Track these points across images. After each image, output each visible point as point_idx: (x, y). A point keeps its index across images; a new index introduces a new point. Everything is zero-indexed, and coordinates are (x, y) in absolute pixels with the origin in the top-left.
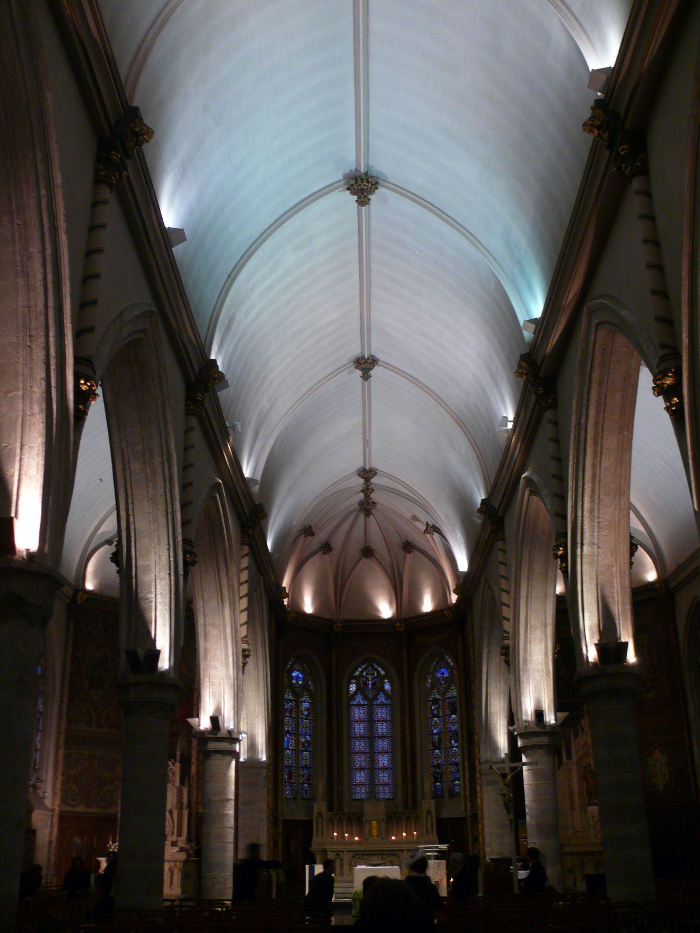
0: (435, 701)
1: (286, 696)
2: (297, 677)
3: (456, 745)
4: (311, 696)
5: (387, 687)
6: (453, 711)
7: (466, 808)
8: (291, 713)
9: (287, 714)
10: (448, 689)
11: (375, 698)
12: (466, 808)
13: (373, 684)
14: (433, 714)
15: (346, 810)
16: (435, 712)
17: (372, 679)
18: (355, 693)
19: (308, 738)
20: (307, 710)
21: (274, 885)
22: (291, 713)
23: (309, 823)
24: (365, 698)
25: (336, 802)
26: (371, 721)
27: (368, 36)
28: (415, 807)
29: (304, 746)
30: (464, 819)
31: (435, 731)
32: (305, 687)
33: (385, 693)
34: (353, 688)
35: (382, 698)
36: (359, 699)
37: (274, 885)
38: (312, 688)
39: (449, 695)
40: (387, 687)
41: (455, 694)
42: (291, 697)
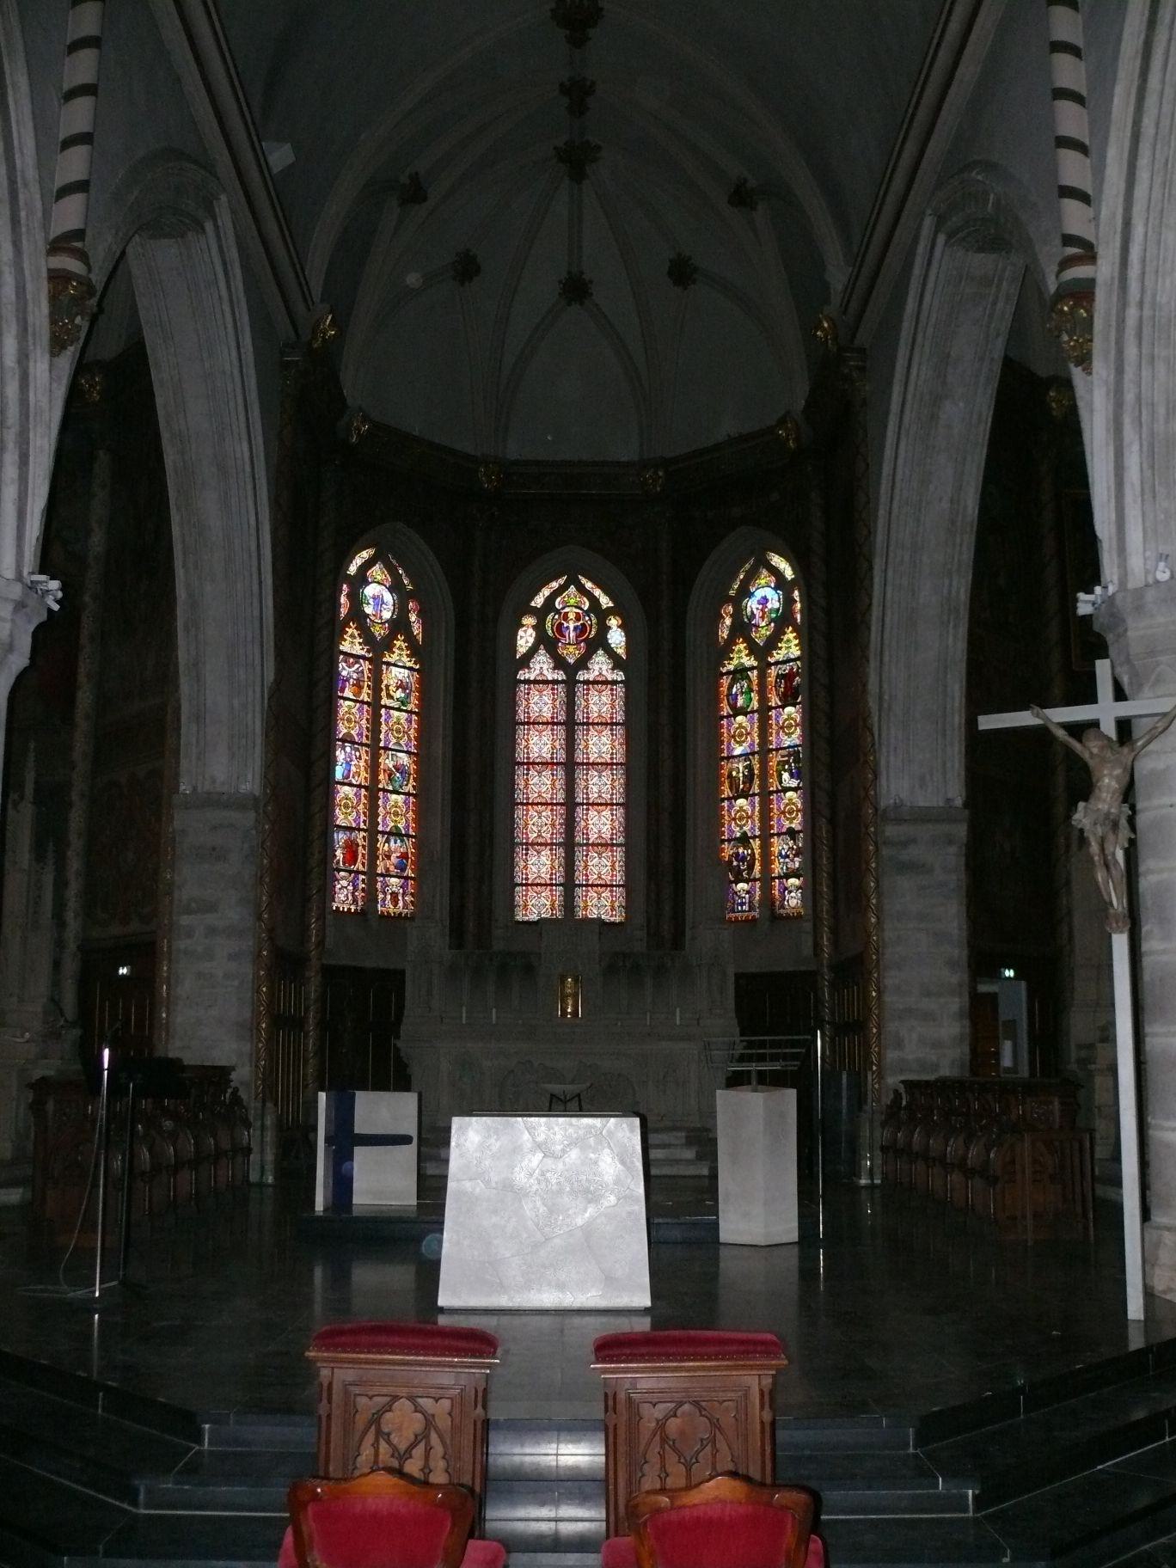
0: (741, 672)
1: (345, 647)
2: (378, 600)
3: (794, 783)
4: (415, 650)
5: (617, 638)
6: (788, 699)
7: (817, 946)
8: (358, 685)
9: (348, 693)
10: (773, 642)
11: (583, 663)
12: (817, 946)
13: (581, 630)
14: (733, 706)
15: (498, 946)
16: (740, 702)
17: (578, 618)
18: (533, 651)
19: (404, 759)
20: (401, 686)
21: (76, 843)
22: (358, 685)
23: (394, 979)
24: (559, 663)
25: (471, 925)
26: (571, 725)
27: (679, 739)
28: (678, 941)
29: (391, 778)
30: (811, 977)
31: (738, 751)
32: (399, 625)
33: (610, 653)
34: (525, 638)
35: (600, 665)
36: (542, 666)
37: (76, 843)
38: (417, 629)
39: (778, 656)
40: (617, 638)
41: (795, 652)
42: (358, 650)
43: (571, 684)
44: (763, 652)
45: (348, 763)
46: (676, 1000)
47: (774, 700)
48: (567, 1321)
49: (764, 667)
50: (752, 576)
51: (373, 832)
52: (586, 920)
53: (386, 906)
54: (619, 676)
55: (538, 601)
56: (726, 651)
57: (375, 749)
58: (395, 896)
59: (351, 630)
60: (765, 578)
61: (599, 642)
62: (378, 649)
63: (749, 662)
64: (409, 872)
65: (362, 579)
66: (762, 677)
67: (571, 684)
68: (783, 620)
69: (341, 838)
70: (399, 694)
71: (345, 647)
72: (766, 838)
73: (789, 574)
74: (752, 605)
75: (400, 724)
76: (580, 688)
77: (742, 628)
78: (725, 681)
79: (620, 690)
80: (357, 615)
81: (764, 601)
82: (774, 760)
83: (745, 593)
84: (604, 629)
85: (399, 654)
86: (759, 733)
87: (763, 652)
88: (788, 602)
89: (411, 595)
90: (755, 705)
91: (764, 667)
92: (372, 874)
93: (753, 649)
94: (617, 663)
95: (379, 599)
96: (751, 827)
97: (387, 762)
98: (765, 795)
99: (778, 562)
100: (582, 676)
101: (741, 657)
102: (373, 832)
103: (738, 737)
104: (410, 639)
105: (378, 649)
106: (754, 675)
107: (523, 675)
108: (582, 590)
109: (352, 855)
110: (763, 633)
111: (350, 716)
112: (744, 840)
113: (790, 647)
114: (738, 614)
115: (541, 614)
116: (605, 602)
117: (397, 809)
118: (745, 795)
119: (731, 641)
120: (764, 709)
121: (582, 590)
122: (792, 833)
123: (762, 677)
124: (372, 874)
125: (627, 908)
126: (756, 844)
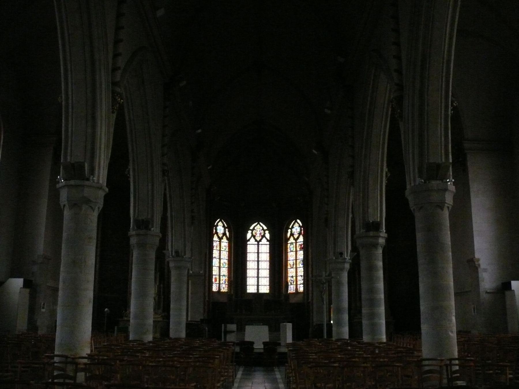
0: (292, 243)
4: (227, 239)
10: (298, 238)
11: (260, 240)
20: (225, 246)
22: (217, 247)
32: (224, 234)
34: (249, 235)
35: (264, 241)
36: (252, 241)
41: (302, 240)
43: (258, 245)
44: (296, 240)
45: (215, 262)
46: (271, 346)
47: (298, 249)
48: (61, 354)
49: (296, 243)
50: (294, 224)
51: (220, 275)
52: (264, 349)
53: (222, 290)
54: (268, 243)
55: (251, 228)
56: (289, 239)
57: (220, 259)
58: (224, 288)
59: (215, 236)
60: (296, 224)
61: (263, 236)
62: (220, 239)
63: (294, 241)
64: (227, 283)
65: (217, 225)
66: (296, 244)
67: (258, 245)
68: (300, 234)
69: (214, 277)
70: (225, 248)
71: (214, 239)
72: (296, 276)
73: (301, 225)
74: (294, 230)
75: (225, 255)
76: (260, 246)
77: (292, 235)
78: (289, 245)
79: (268, 246)
80: (217, 233)
81: (297, 229)
82: (298, 261)
83: (293, 227)
84: (265, 233)
85: (225, 240)
86: (295, 255)
87: (296, 240)
88: (301, 230)
89: (227, 228)
90: (295, 250)
91: (296, 243)
92: (219, 284)
93: (294, 239)
94: (268, 241)
95: (220, 229)
96: (294, 274)
97: (222, 261)
98: (296, 268)
99: (298, 221)
100: (260, 243)
101: (292, 240)
102: (220, 275)
103: (292, 256)
104: (226, 237)
105: (220, 239)
106: (294, 244)
107: (248, 243)
108: (260, 225)
109: (216, 281)
110: (296, 236)
111: (216, 253)
112: (292, 277)
113: (301, 239)
114: (291, 232)
115: (252, 230)
116: (265, 228)
117: (225, 271)
118: (292, 268)
119: (290, 237)
120: (296, 251)
121: (260, 225)
122: (301, 276)
123: (296, 244)
124: (219, 284)
125: (270, 290)
126: (295, 278)
